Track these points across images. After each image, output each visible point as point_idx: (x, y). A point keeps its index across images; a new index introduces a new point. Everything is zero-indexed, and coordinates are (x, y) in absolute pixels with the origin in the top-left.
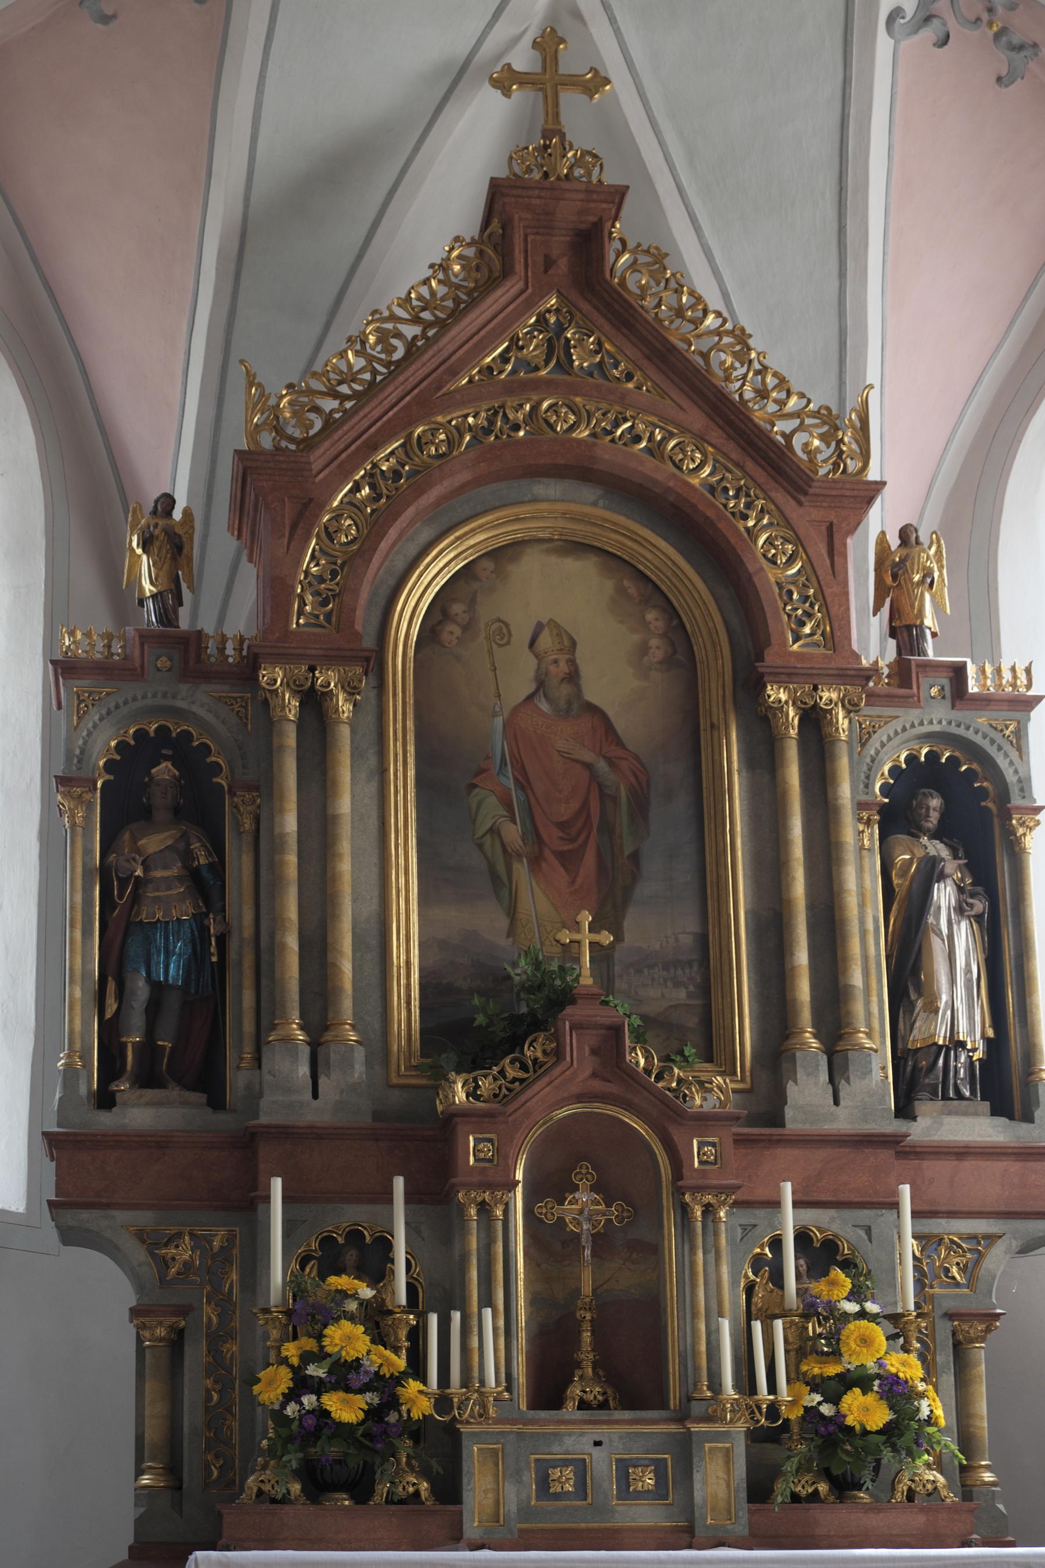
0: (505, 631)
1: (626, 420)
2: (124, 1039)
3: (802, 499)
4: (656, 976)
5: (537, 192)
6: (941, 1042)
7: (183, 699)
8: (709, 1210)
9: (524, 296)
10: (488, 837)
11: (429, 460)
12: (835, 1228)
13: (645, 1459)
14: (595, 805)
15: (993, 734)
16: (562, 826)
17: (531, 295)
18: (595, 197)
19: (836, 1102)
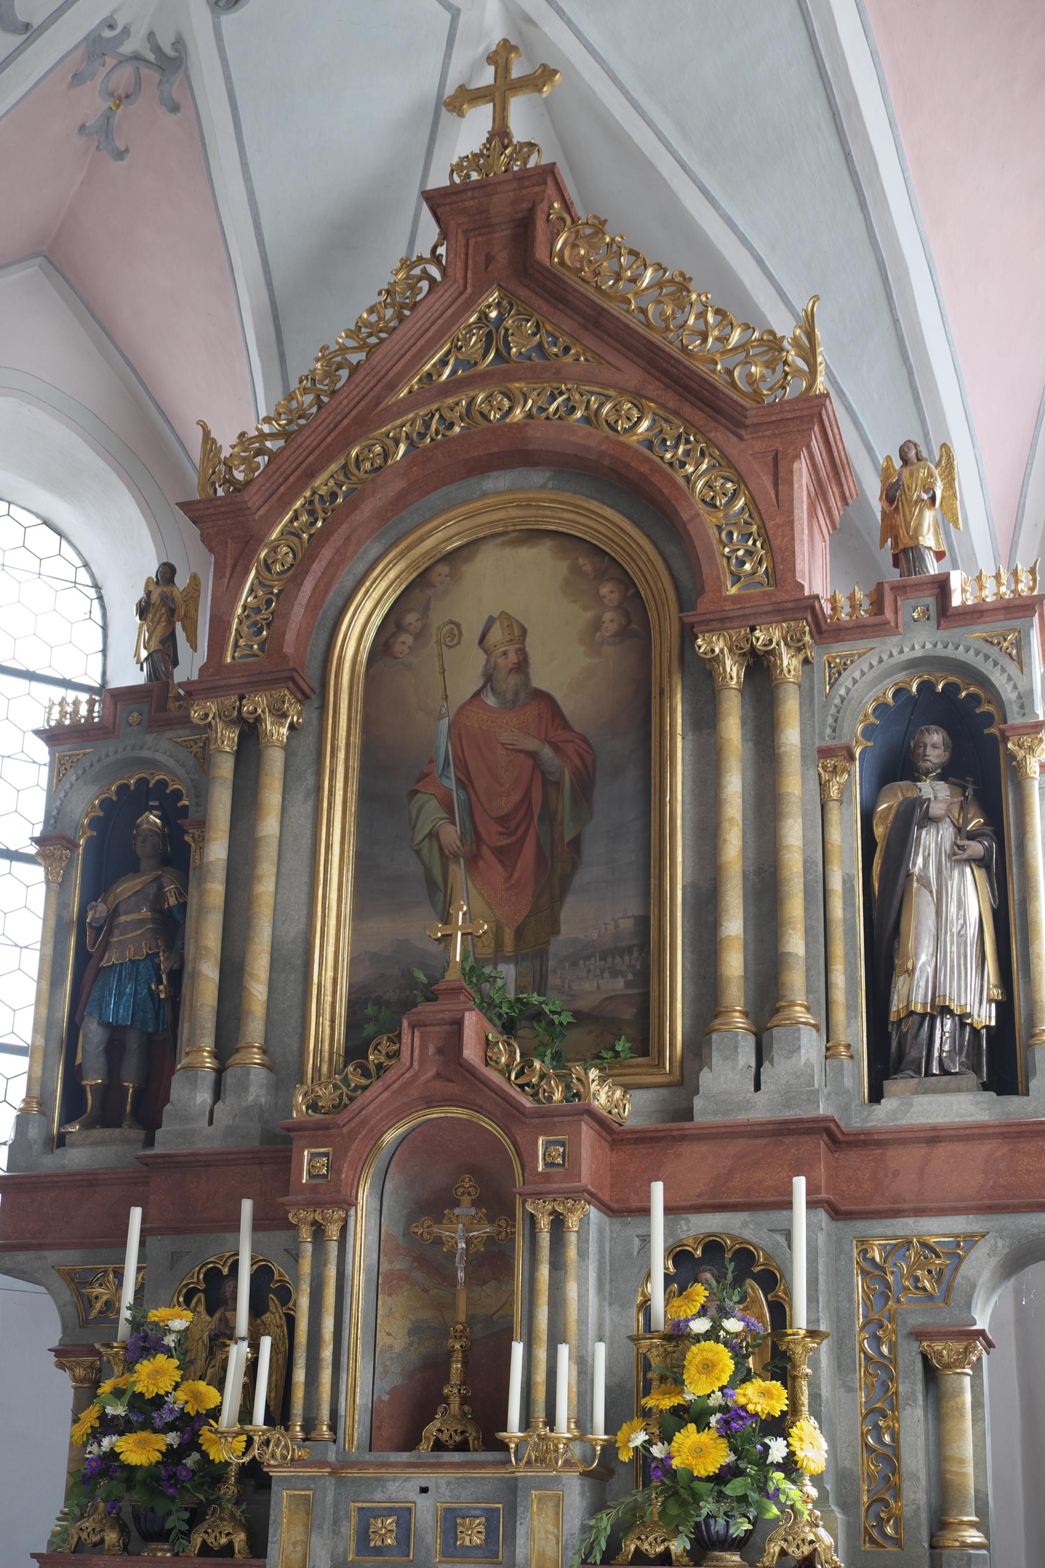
0: (456, 632)
1: (561, 393)
2: (85, 1082)
3: (743, 432)
4: (592, 968)
5: (470, 194)
6: (919, 1009)
7: (149, 749)
8: (558, 1223)
9: (463, 298)
10: (426, 844)
11: (366, 476)
12: (748, 1234)
13: (477, 1508)
14: (537, 795)
15: (987, 649)
16: (501, 820)
17: (471, 295)
18: (526, 183)
19: (757, 1087)
